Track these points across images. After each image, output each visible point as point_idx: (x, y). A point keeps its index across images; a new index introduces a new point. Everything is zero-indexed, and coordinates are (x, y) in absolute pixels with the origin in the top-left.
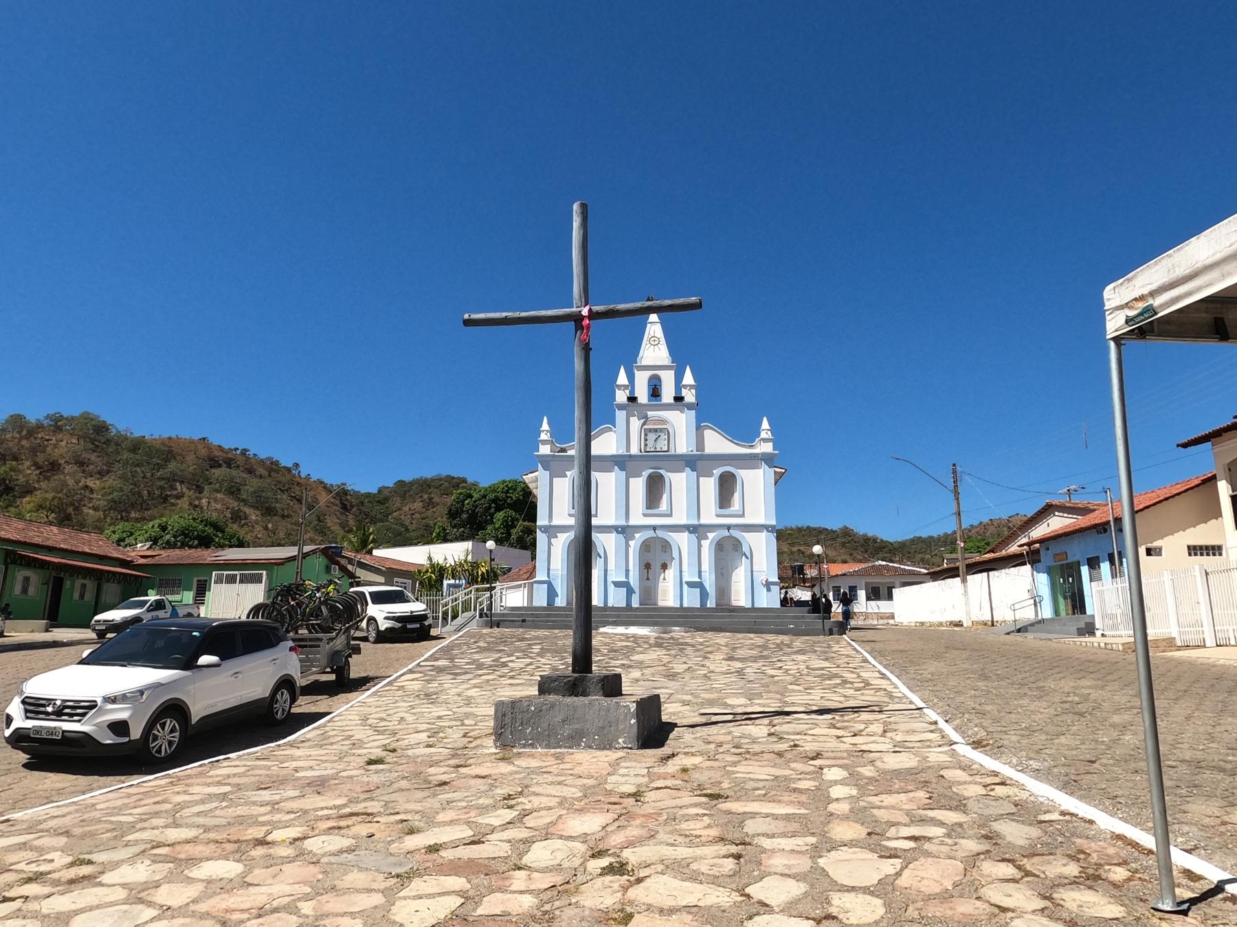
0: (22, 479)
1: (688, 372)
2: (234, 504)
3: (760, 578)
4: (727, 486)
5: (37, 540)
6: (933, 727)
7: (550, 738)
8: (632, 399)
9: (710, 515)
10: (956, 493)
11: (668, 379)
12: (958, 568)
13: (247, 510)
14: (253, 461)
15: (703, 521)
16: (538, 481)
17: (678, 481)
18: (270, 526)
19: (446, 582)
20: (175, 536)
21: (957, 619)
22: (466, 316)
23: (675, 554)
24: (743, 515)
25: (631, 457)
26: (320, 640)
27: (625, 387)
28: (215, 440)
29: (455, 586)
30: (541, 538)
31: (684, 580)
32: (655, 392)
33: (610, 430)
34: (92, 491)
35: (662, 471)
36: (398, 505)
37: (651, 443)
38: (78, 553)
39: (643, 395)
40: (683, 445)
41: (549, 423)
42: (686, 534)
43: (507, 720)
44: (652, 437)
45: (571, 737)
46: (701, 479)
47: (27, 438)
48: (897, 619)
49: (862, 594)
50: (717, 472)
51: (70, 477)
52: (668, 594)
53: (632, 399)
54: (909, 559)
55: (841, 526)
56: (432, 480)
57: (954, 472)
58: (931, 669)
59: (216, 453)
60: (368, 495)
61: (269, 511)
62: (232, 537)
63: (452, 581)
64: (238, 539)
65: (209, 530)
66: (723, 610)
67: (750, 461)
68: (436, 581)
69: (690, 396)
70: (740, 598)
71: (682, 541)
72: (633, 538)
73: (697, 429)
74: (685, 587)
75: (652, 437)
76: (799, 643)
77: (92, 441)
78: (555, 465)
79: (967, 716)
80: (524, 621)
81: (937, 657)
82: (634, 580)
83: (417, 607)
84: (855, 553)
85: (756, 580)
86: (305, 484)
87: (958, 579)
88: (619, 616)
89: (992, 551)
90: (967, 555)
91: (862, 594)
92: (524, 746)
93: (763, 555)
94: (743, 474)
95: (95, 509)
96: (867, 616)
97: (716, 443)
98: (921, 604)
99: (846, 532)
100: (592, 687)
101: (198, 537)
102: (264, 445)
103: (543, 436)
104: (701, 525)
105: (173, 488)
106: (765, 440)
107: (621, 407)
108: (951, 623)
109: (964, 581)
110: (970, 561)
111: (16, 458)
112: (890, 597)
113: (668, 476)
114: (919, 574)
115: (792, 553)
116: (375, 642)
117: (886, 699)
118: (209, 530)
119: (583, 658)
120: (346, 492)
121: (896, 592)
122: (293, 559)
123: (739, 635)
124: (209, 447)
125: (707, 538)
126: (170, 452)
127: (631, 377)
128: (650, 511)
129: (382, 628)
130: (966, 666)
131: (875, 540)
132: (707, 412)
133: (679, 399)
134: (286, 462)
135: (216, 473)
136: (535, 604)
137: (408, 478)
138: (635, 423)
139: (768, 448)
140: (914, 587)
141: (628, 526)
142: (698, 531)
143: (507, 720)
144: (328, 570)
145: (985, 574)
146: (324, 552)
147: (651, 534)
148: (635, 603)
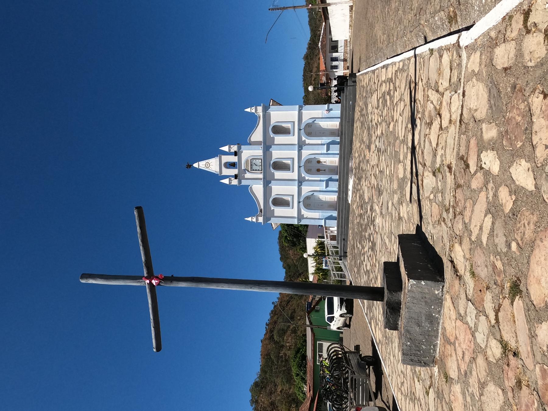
1: (222, 149)
2: (289, 332)
4: (279, 130)
6: (436, 54)
7: (431, 336)
8: (236, 177)
9: (293, 139)
10: (284, 8)
11: (226, 159)
12: (323, 8)
14: (271, 321)
15: (296, 143)
16: (275, 223)
17: (277, 154)
18: (299, 318)
19: (324, 267)
20: (301, 371)
21: (349, 8)
22: (155, 350)
23: (313, 156)
24: (294, 122)
25: (264, 178)
26: (352, 378)
27: (230, 180)
28: (262, 337)
29: (326, 263)
30: (303, 222)
31: (326, 152)
32: (232, 165)
33: (251, 188)
34: (283, 389)
35: (272, 162)
37: (258, 168)
39: (234, 171)
40: (258, 152)
42: (303, 151)
43: (416, 359)
44: (254, 167)
45: (431, 323)
48: (348, 38)
49: (335, 55)
50: (272, 135)
51: (277, 398)
52: (333, 160)
53: (236, 177)
55: (303, 60)
56: (280, 245)
57: (273, 9)
58: (380, 33)
60: (286, 273)
62: (302, 345)
63: (324, 264)
64: (303, 342)
65: (299, 355)
66: (342, 134)
67: (267, 118)
68: (323, 272)
69: (234, 148)
70: (335, 124)
71: (306, 153)
72: (304, 177)
74: (329, 152)
75: (254, 167)
76: (360, 103)
77: (262, 388)
78: (268, 215)
79: (422, 22)
80: (344, 240)
81: (371, 26)
82: (325, 178)
84: (316, 54)
85: (327, 116)
87: (328, 8)
88: (343, 192)
90: (317, 3)
91: (335, 55)
92: (435, 351)
93: (314, 112)
95: (290, 388)
96: (345, 52)
97: (257, 135)
99: (306, 57)
100: (394, 298)
101: (302, 360)
103: (254, 220)
105: (282, 357)
106: (256, 110)
107: (240, 182)
108: (350, 11)
109: (329, 5)
112: (337, 42)
114: (325, 26)
117: (405, 75)
118: (299, 355)
119: (374, 294)
122: (312, 329)
123: (355, 132)
124: (265, 339)
125: (305, 140)
126: (267, 355)
127: (226, 177)
128: (291, 169)
129: (346, 311)
130: (379, 12)
131: (310, 44)
132: (243, 140)
133: (236, 154)
134: (272, 307)
135: (275, 337)
136: (336, 189)
137: (279, 256)
138: (248, 175)
139: (260, 109)
141: (298, 180)
142: (301, 145)
143: (416, 359)
146: (309, 313)
147: (302, 169)
148: (337, 177)
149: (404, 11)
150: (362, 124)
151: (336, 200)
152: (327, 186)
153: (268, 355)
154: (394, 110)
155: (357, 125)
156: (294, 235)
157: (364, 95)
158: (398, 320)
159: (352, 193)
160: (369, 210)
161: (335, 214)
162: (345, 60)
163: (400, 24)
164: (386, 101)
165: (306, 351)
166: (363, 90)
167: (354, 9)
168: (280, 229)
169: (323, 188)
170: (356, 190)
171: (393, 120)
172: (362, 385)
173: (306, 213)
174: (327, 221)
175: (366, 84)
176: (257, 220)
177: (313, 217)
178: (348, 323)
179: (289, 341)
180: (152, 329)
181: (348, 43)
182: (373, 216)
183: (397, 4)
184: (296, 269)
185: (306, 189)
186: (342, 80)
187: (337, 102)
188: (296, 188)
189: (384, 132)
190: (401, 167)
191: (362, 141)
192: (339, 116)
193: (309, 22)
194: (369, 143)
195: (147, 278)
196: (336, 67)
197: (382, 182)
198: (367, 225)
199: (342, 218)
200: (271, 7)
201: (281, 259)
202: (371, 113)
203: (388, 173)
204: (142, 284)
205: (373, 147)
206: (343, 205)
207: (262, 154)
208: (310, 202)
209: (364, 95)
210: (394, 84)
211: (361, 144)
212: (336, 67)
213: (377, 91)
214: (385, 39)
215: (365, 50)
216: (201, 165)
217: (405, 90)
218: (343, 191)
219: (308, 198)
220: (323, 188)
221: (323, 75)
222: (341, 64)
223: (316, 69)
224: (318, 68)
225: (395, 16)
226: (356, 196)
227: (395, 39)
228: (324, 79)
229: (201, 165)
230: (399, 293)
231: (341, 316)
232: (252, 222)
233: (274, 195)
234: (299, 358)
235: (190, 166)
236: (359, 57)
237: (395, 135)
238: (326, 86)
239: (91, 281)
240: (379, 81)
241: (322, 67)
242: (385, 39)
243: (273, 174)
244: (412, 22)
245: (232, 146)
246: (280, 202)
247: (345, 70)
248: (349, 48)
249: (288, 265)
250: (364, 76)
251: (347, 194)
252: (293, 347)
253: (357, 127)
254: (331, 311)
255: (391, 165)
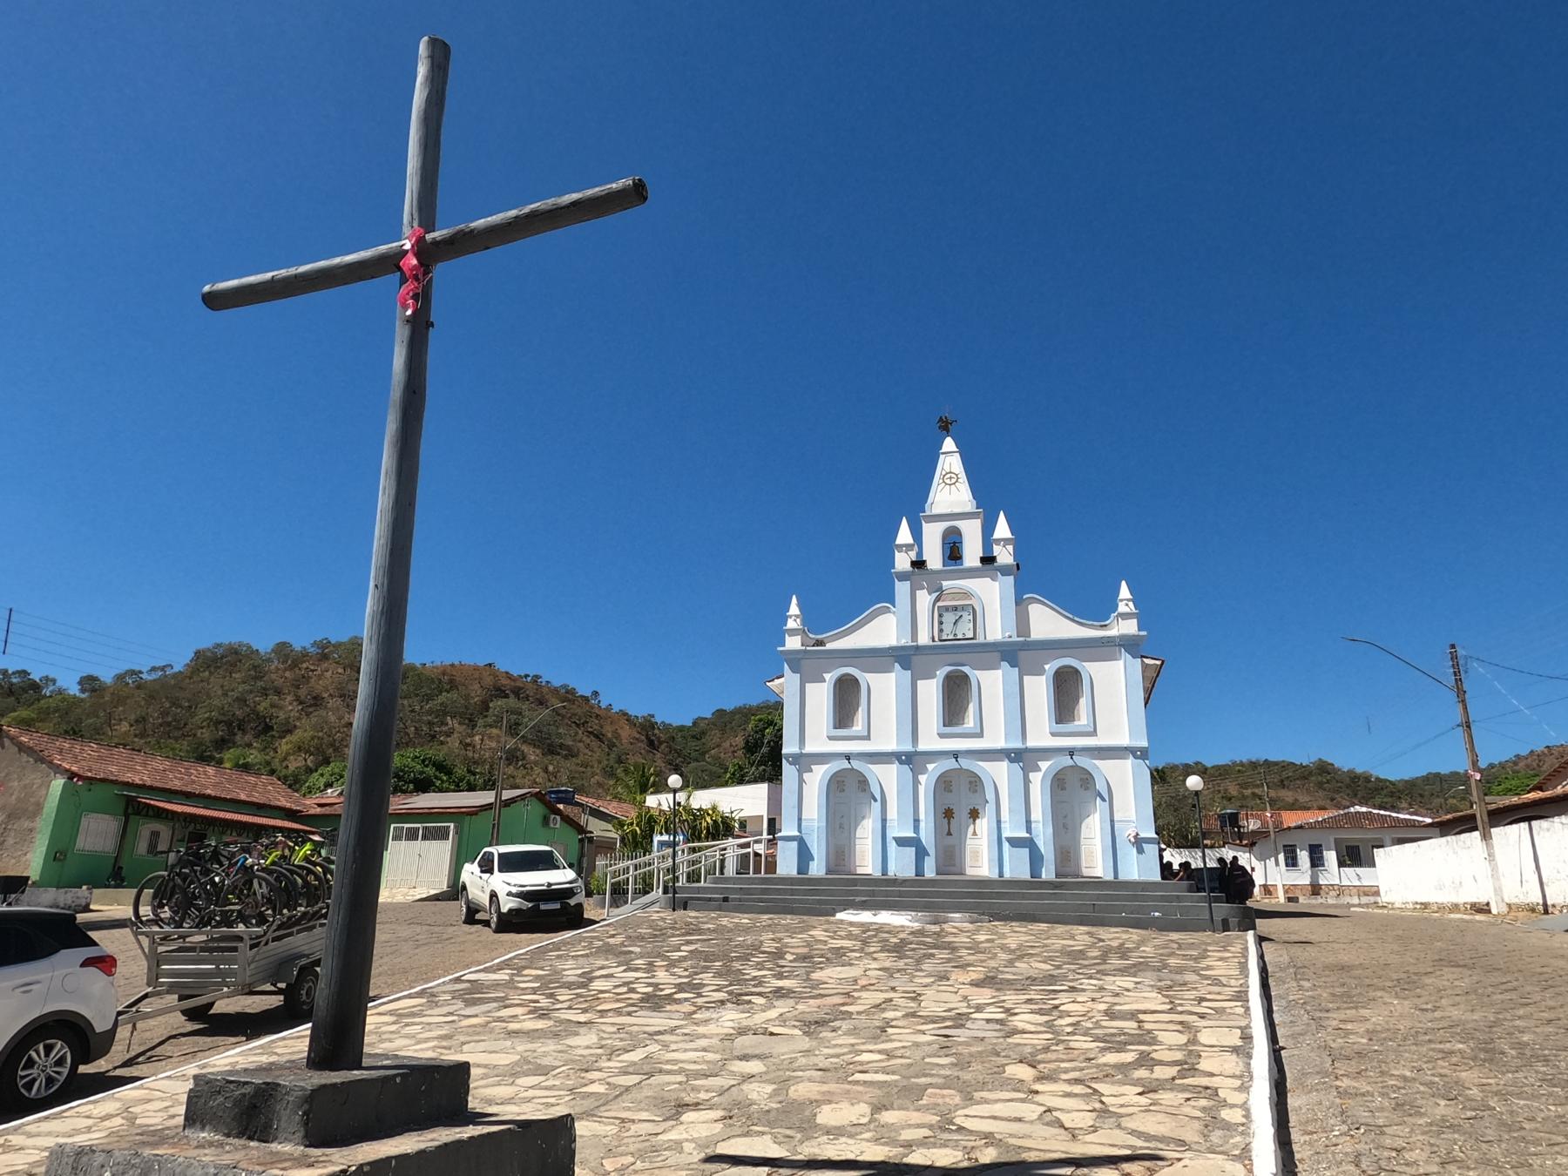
0: (282, 715)
3: (1126, 832)
4: (1067, 689)
5: (176, 784)
8: (919, 564)
9: (1041, 734)
10: (1461, 693)
12: (1473, 817)
13: (525, 748)
14: (545, 690)
15: (1031, 743)
16: (786, 685)
17: (991, 683)
18: (551, 768)
19: (657, 838)
21: (1483, 900)
22: (207, 288)
23: (990, 796)
24: (1094, 733)
27: (909, 547)
28: (502, 666)
30: (788, 771)
32: (953, 552)
33: (887, 610)
35: (966, 669)
36: (716, 740)
37: (948, 628)
38: (225, 799)
39: (934, 560)
40: (996, 628)
41: (799, 605)
42: (1005, 764)
46: (1026, 678)
47: (291, 668)
48: (1384, 898)
49: (1331, 857)
52: (982, 857)
53: (919, 564)
54: (1422, 804)
57: (1454, 657)
58: (1376, 1017)
59: (504, 681)
60: (681, 729)
61: (551, 750)
62: (461, 780)
63: (665, 838)
64: (469, 783)
65: (430, 771)
69: (1005, 556)
70: (1095, 864)
71: (1000, 774)
72: (924, 771)
73: (1017, 604)
74: (1006, 845)
75: (949, 618)
78: (806, 665)
80: (726, 900)
81: (1407, 985)
82: (927, 835)
83: (562, 876)
85: (1119, 837)
86: (604, 716)
87: (1476, 834)
88: (873, 894)
89: (1539, 788)
91: (1331, 857)
93: (1129, 797)
94: (1093, 670)
96: (1341, 890)
97: (1047, 623)
98: (1421, 874)
100: (285, 1115)
102: (559, 668)
103: (791, 624)
104: (1027, 750)
105: (444, 723)
106: (1125, 616)
107: (903, 576)
109: (1486, 837)
110: (1494, 806)
111: (278, 692)
112: (1371, 863)
113: (975, 675)
115: (1244, 797)
116: (496, 931)
117: (1190, 1134)
118: (430, 771)
120: (653, 726)
121: (1379, 854)
122: (489, 807)
123: (1060, 929)
126: (451, 681)
128: (948, 730)
129: (504, 910)
130: (1455, 1013)
131: (1367, 779)
132: (1031, 579)
133: (988, 560)
134: (584, 690)
135: (497, 704)
136: (893, 870)
137: (729, 706)
138: (925, 599)
139: (1130, 627)
140: (1407, 845)
141: (916, 753)
142: (1022, 757)
144: (546, 821)
145: (1524, 825)
146: (539, 796)
147: (950, 764)
148: (930, 873)
149: (1443, 1125)
150: (1076, 956)
151: (860, 871)
152: (902, 842)
153: (453, 685)
154: (1077, 1081)
155: (1080, 936)
156: (759, 751)
157: (1172, 961)
158: (216, 1130)
159: (862, 925)
160: (780, 983)
161: (817, 869)
162: (1316, 889)
163: (1398, 1106)
164: (1120, 1048)
165: (441, 791)
166: (1191, 958)
167: (1479, 917)
168: (773, 700)
169: (895, 831)
170: (867, 935)
171: (1041, 1078)
172: (218, 973)
173: (818, 776)
174: (795, 844)
175: (1208, 968)
176: (793, 632)
177: (808, 796)
178: (478, 916)
179: (490, 742)
180: (269, 275)
181: (1372, 899)
182: (755, 999)
183: (1474, 1092)
184: (694, 754)
185: (888, 777)
186: (1233, 883)
187: (1166, 869)
188: (891, 746)
189: (1016, 1039)
190: (856, 1112)
191: (1020, 954)
192: (1122, 877)
193: (1437, 775)
194: (1003, 981)
195: (420, 241)
196: (1292, 862)
197: (848, 1033)
198: (736, 977)
199: (793, 892)
200: (1461, 652)
201: (720, 713)
202: (1102, 989)
203: (865, 1057)
204: (407, 231)
205: (984, 996)
206: (831, 893)
207: (991, 638)
208: (849, 790)
209: (1172, 961)
210: (1169, 1084)
211: (1012, 951)
212: (1292, 862)
213: (1171, 1011)
214: (1353, 1038)
215: (1331, 960)
216: (950, 460)
217: (1133, 1132)
218: (883, 893)
219: (863, 783)
220: (895, 831)
221: (1264, 823)
222: (1302, 875)
223: (1290, 800)
224: (1293, 807)
225: (1430, 1084)
226: (850, 936)
227: (1345, 1083)
228: (1253, 825)
229: (950, 460)
230: (300, 1134)
231: (493, 896)
232: (786, 618)
233: (867, 679)
234: (422, 773)
235: (945, 427)
236: (1311, 938)
237: (983, 1086)
238: (1231, 829)
239: (422, 70)
240: (1202, 1016)
241: (1291, 819)
242: (1353, 1038)
243: (932, 676)
244: (1393, 1165)
245: (1010, 548)
246: (847, 698)
247: (1286, 892)
248: (1355, 901)
249: (703, 733)
250: (1234, 959)
251: (863, 906)
252: (470, 754)
253: (1072, 937)
254: (513, 863)
255: (885, 1071)
